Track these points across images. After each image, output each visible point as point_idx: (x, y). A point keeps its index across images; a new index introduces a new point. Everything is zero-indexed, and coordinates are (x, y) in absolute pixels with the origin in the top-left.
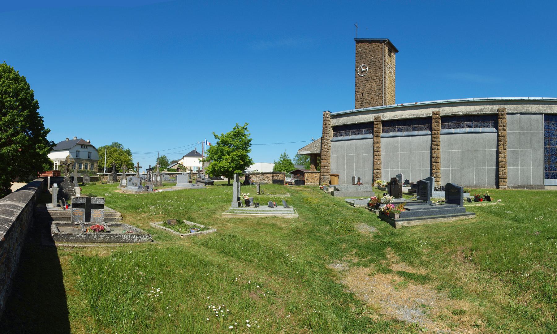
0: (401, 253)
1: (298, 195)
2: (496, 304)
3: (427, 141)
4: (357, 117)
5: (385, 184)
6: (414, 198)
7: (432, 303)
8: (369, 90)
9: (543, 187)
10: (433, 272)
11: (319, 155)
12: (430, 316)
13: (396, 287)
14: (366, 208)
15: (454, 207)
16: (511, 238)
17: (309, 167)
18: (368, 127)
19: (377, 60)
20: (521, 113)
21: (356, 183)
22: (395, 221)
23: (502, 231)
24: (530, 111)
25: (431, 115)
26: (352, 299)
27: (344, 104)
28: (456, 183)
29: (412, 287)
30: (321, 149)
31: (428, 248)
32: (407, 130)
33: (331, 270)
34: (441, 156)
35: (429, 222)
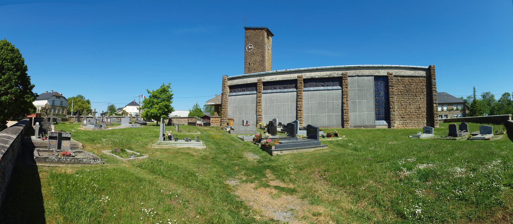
0: (276, 173)
1: (205, 133)
2: (342, 210)
4: (245, 79)
5: (265, 125)
6: (285, 135)
7: (298, 208)
8: (254, 61)
9: (374, 126)
10: (298, 186)
11: (220, 105)
12: (296, 217)
13: (273, 197)
15: (313, 141)
16: (352, 163)
17: (213, 114)
18: (253, 86)
20: (358, 76)
23: (345, 157)
24: (365, 74)
26: (242, 205)
27: (237, 71)
28: (314, 125)
29: (284, 196)
31: (295, 170)
32: (280, 89)
33: (228, 185)
34: (304, 106)
35: (295, 152)
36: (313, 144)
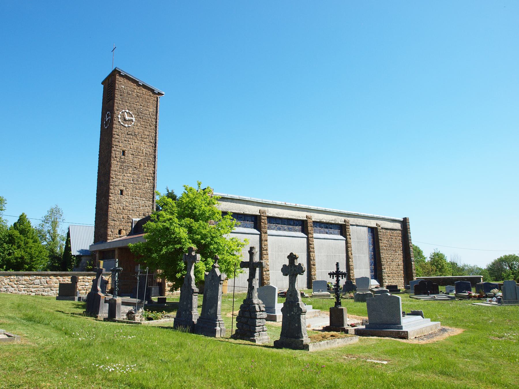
20: (357, 225)
25: (305, 219)
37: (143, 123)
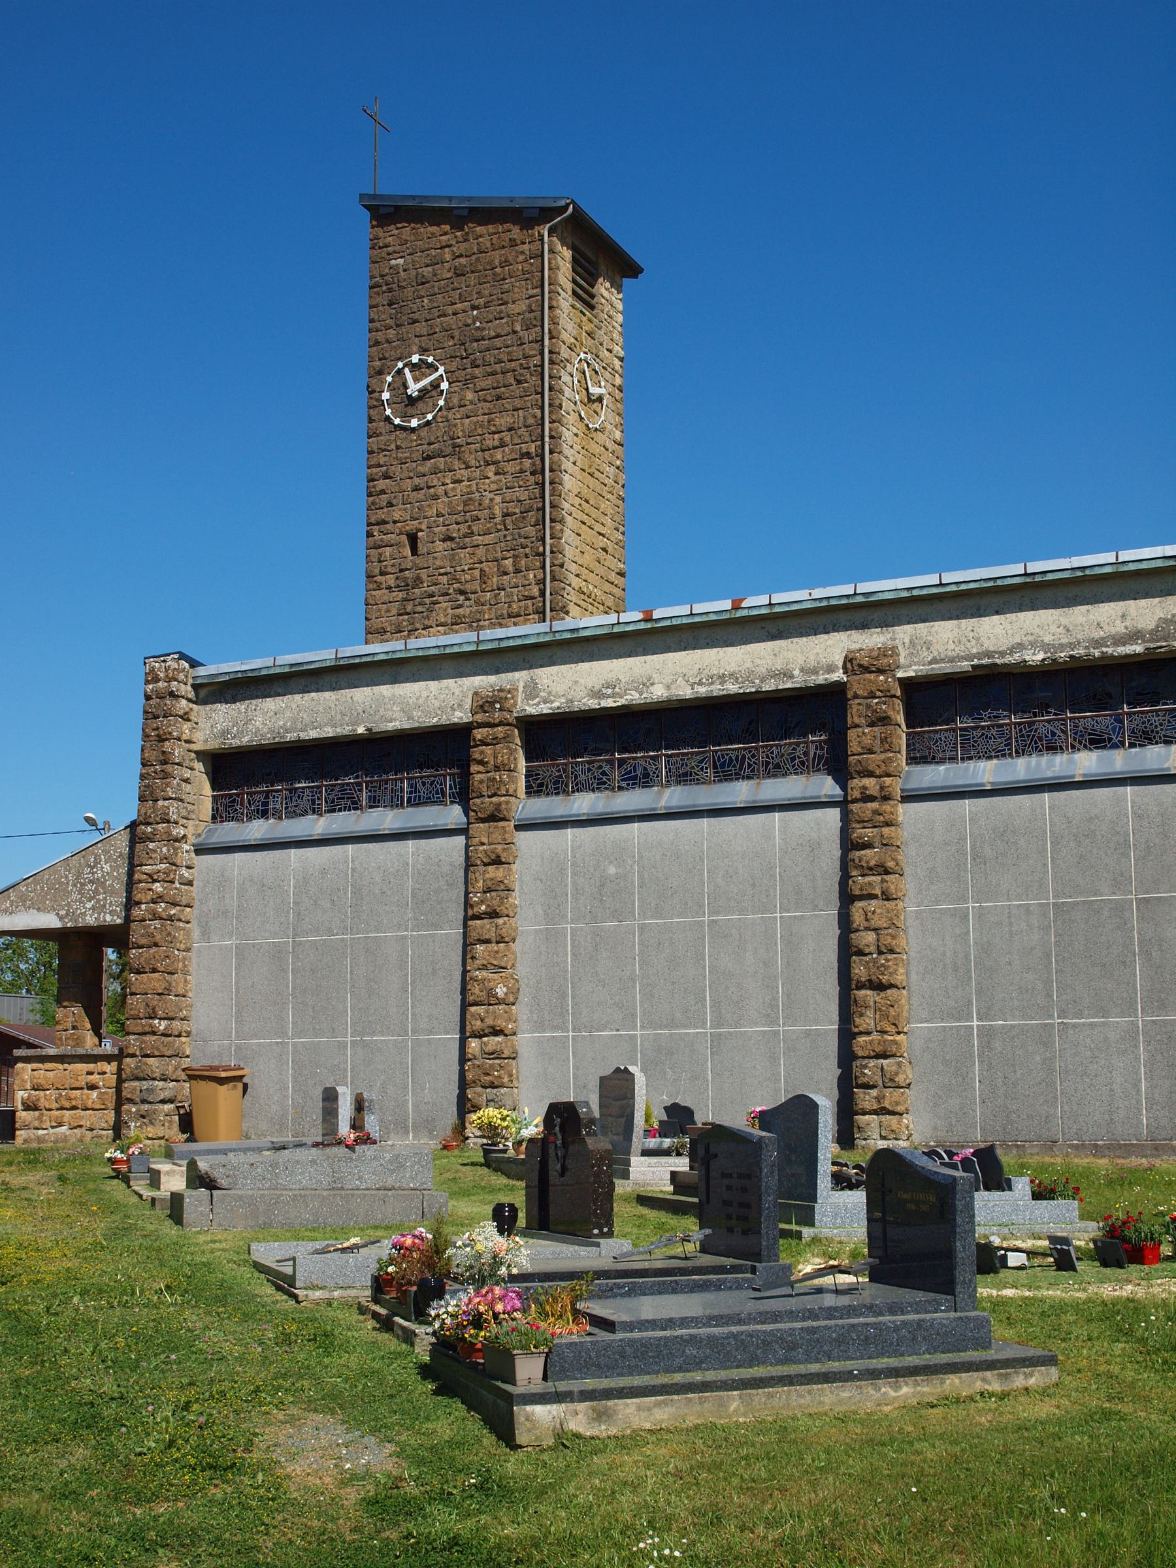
3: (814, 847)
4: (362, 696)
8: (455, 521)
11: (118, 936)
14: (362, 1310)
15: (919, 1309)
18: (434, 758)
19: (502, 326)
21: (344, 1129)
22: (510, 1399)
25: (838, 676)
27: (291, 608)
30: (130, 904)
32: (683, 778)
35: (736, 1408)
36: (916, 1336)
37: (489, 381)
